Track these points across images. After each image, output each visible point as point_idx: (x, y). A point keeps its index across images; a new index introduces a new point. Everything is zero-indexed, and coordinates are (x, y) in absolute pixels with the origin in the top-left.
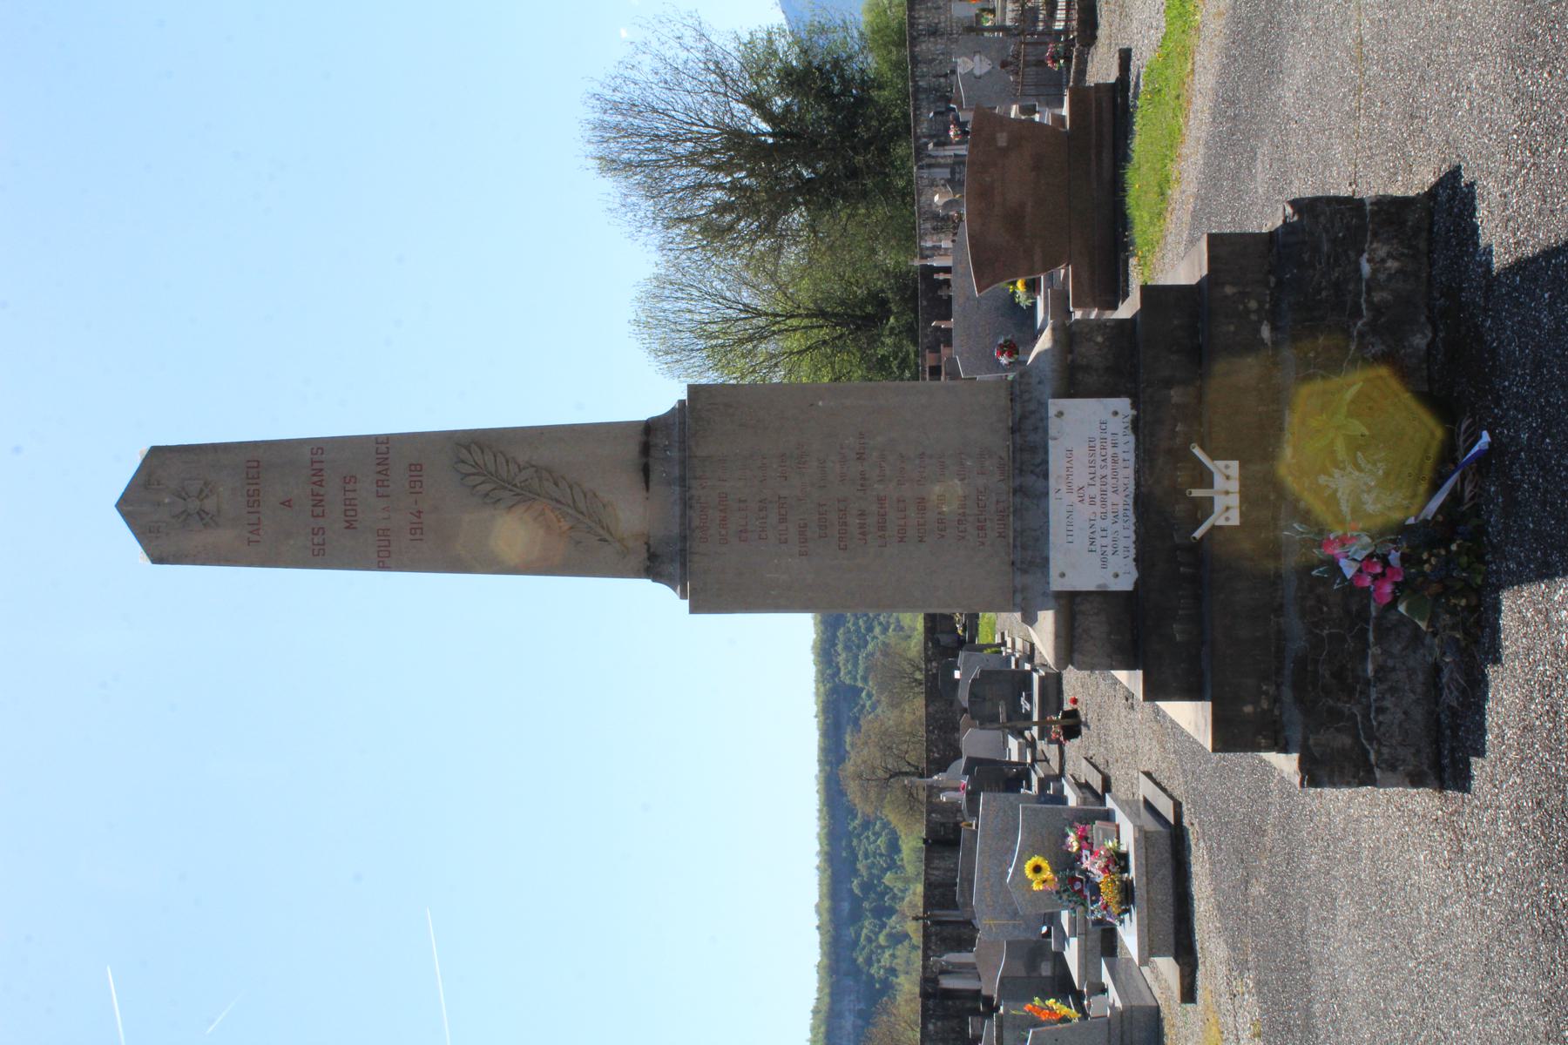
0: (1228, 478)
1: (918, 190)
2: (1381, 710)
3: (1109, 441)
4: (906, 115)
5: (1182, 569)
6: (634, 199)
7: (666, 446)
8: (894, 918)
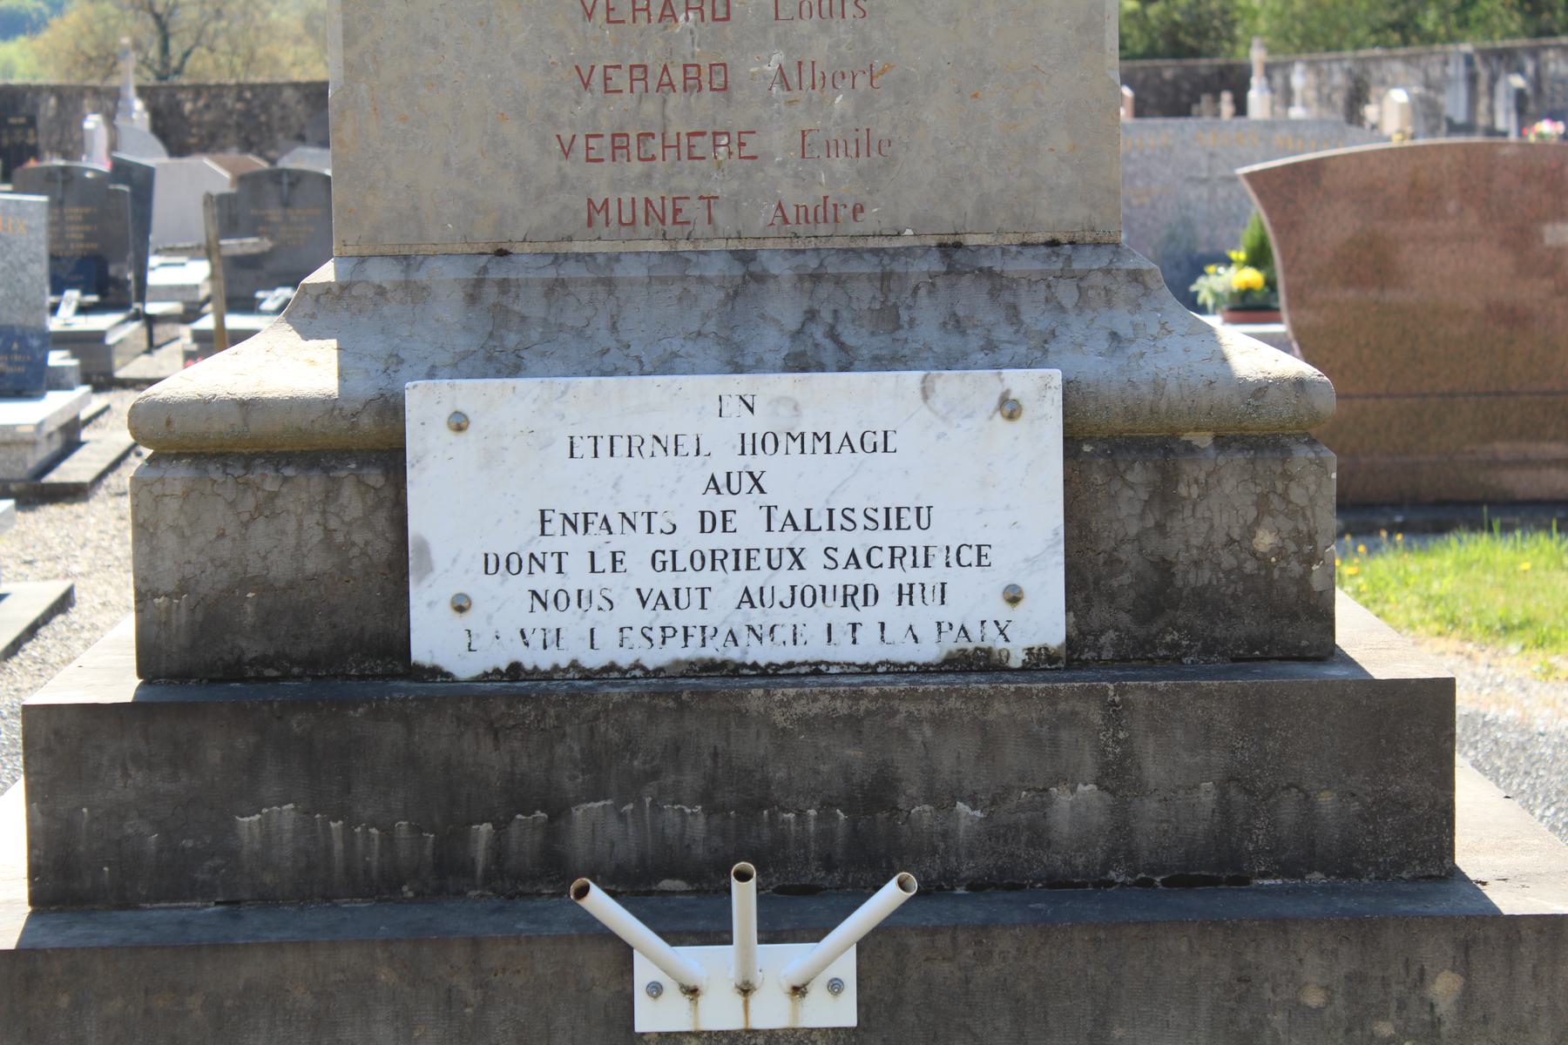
0: (798, 991)
1: (1418, 56)
3: (918, 575)
5: (486, 828)
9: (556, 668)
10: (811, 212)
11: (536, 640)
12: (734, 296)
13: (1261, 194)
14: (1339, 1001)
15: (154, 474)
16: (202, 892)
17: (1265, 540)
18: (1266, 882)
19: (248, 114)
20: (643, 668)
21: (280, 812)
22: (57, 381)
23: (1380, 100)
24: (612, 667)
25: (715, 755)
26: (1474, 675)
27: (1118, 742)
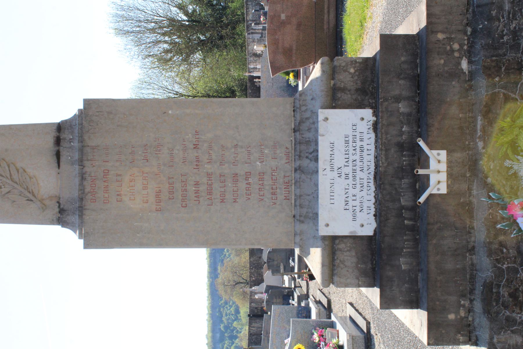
0: (439, 162)
3: (358, 138)
4: (243, 14)
5: (406, 222)
6: (130, 47)
7: (71, 139)
8: (237, 340)
9: (375, 208)
10: (287, 157)
11: (369, 211)
12: (303, 172)
13: (276, 73)
14: (443, 57)
15: (336, 283)
16: (417, 276)
17: (352, 70)
18: (419, 71)
19: (255, 267)
20: (375, 191)
21: (402, 261)
22: (308, 304)
23: (256, 51)
24: (375, 197)
25: (392, 177)
26: (371, 32)
27: (391, 99)
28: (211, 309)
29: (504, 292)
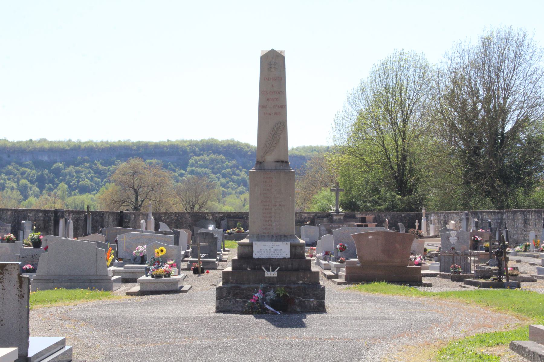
0: (274, 274)
1: (458, 213)
2: (230, 301)
4: (508, 206)
8: (37, 189)
19: (177, 220)
28: (88, 147)
29: (238, 291)
